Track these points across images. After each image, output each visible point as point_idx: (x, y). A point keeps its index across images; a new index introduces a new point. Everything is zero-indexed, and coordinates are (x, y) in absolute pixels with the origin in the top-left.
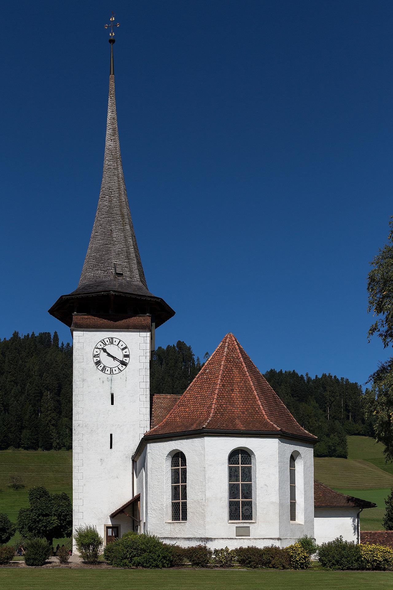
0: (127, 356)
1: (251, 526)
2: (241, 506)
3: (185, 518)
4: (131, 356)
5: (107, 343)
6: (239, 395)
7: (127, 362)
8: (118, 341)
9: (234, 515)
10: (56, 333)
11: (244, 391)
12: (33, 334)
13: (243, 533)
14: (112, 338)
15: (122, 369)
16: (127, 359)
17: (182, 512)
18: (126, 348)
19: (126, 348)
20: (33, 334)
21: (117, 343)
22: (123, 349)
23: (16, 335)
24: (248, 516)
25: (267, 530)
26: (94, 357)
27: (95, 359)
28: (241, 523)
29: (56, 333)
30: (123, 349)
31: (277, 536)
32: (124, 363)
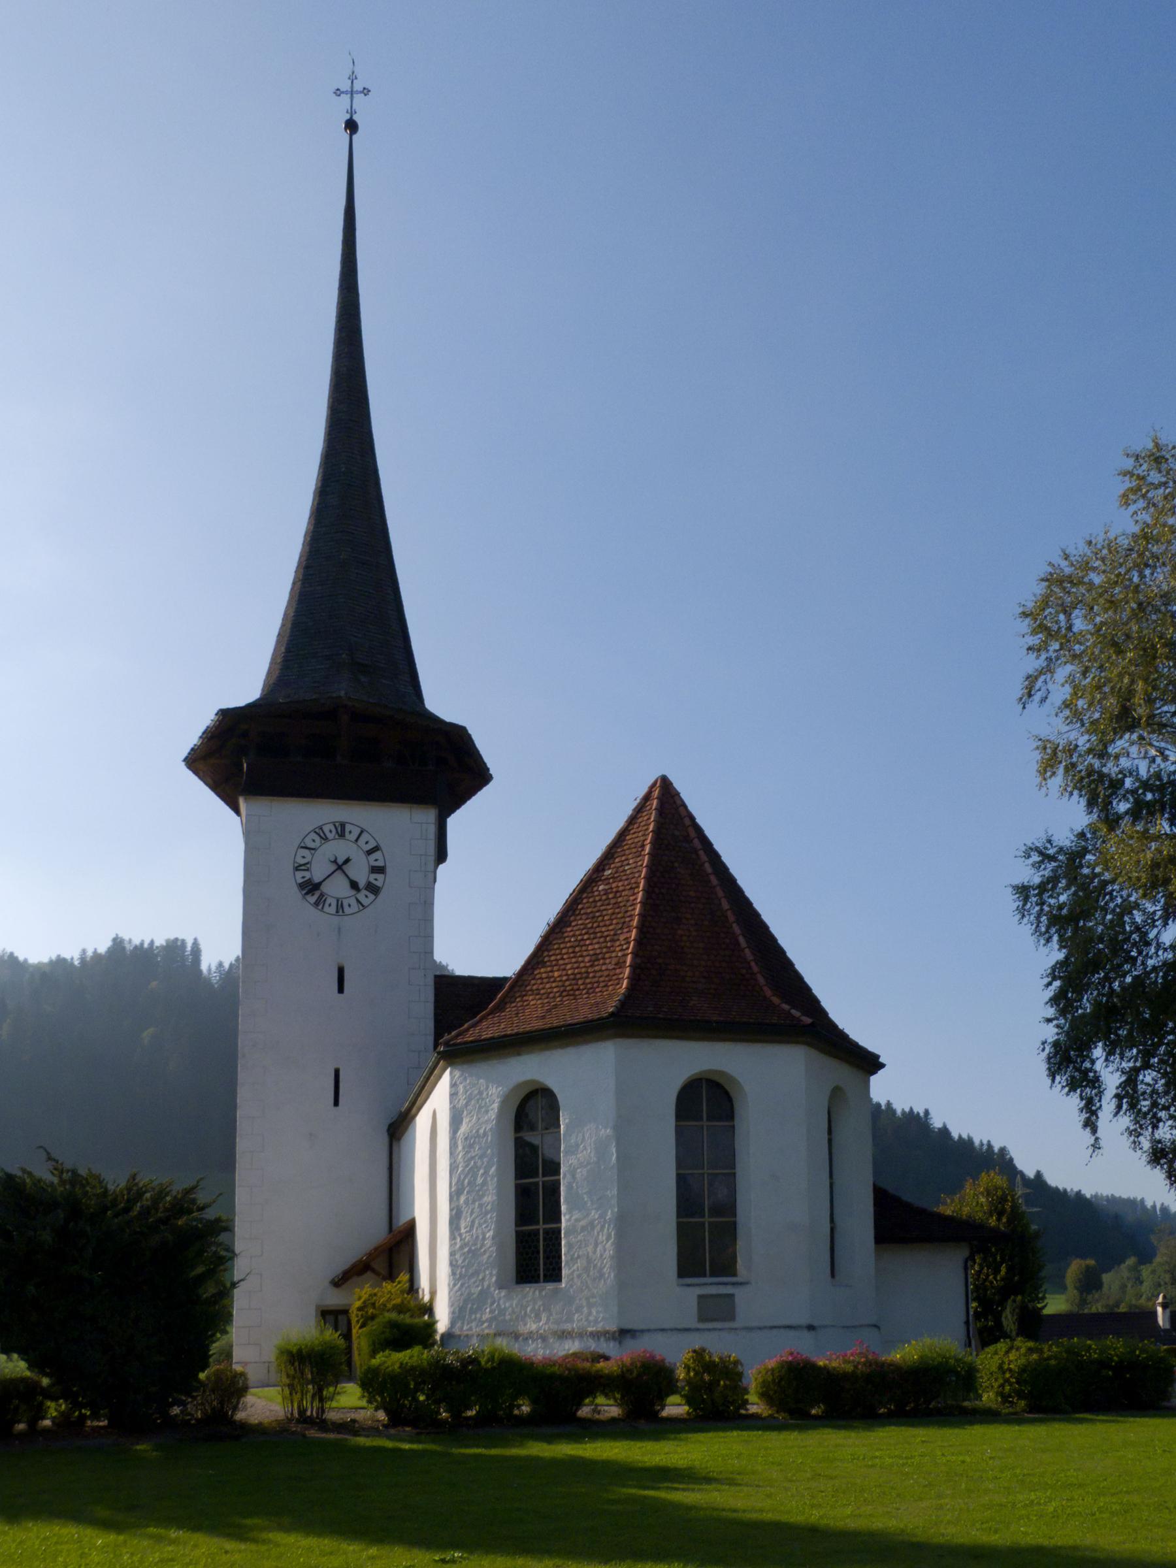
0: (379, 870)
1: (740, 1294)
2: (706, 1238)
3: (554, 1274)
4: (388, 870)
5: (330, 836)
6: (694, 933)
7: (379, 884)
8: (356, 831)
9: (690, 1264)
10: (195, 939)
11: (706, 923)
12: (152, 942)
13: (716, 1311)
14: (343, 825)
15: (365, 902)
16: (380, 877)
17: (547, 1258)
18: (376, 849)
19: (376, 849)
20: (152, 942)
21: (353, 837)
22: (369, 852)
23: (118, 943)
24: (725, 1267)
25: (552, 1327)
26: (297, 869)
27: (299, 874)
28: (712, 1287)
29: (195, 939)
30: (369, 852)
31: (804, 1320)
32: (374, 889)
